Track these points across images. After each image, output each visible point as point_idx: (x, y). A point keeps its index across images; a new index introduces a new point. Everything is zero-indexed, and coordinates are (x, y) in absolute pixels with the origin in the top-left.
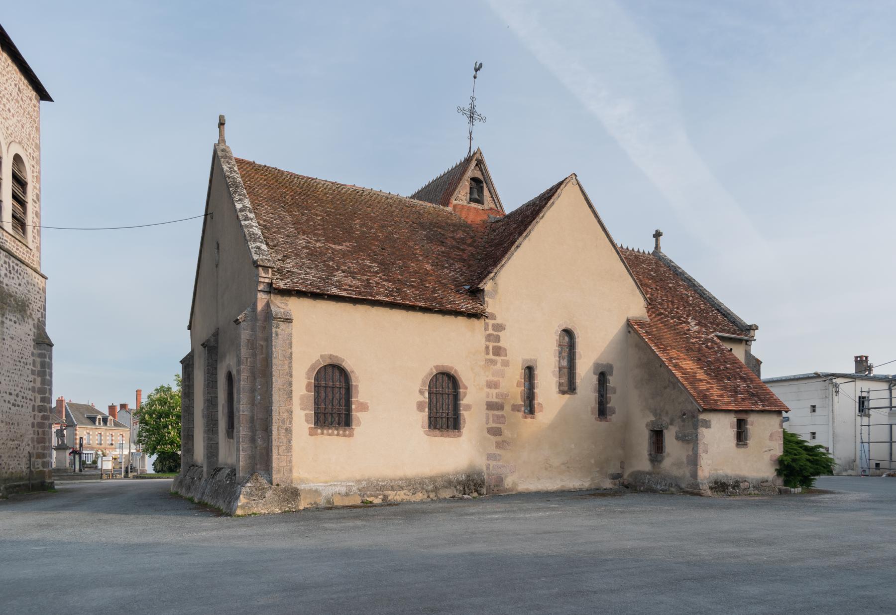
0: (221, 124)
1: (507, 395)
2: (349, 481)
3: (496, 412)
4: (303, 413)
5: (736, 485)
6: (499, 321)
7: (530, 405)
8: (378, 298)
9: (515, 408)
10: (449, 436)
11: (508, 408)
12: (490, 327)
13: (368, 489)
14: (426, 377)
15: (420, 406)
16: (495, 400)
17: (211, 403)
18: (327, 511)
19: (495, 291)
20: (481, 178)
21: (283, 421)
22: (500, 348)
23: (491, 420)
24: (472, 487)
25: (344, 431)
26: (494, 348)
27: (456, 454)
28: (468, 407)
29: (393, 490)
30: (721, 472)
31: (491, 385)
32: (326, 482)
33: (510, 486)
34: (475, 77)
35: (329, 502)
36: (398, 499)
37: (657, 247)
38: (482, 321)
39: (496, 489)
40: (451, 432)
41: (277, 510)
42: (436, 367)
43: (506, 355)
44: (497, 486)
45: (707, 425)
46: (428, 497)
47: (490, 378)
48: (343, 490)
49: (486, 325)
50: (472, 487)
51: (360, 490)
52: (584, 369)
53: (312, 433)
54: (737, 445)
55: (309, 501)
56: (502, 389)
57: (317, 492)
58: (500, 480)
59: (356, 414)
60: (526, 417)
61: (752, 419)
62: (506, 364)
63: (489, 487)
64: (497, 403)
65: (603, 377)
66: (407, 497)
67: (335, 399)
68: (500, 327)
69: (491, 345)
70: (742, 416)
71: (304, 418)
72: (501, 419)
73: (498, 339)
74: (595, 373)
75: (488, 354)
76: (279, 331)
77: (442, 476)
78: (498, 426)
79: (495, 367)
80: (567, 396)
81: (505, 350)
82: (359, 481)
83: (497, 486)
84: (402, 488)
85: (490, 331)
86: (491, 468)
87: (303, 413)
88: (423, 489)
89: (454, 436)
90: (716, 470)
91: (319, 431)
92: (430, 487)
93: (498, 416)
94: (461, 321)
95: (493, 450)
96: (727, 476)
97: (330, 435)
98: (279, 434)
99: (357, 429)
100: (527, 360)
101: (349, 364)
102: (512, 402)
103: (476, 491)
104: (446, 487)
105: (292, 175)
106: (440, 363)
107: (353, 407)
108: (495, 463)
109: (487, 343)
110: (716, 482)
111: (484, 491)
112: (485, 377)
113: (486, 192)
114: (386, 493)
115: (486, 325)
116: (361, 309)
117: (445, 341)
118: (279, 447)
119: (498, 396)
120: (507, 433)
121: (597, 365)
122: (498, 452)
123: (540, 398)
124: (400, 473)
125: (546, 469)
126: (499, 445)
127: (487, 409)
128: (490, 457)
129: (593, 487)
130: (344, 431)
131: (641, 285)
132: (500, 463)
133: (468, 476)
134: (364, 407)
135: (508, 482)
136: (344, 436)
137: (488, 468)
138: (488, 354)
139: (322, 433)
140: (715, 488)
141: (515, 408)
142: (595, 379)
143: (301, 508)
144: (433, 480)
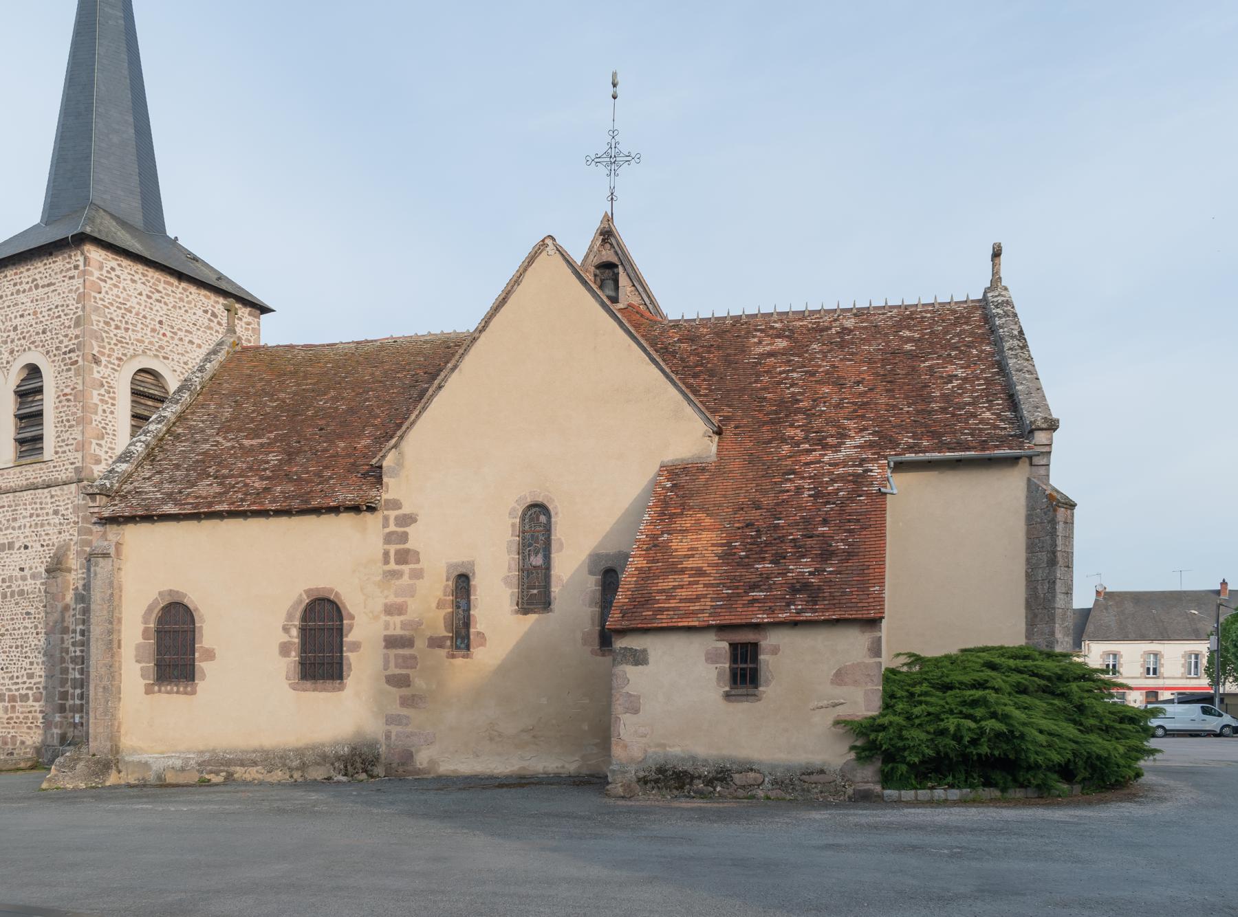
0: (996, 254)
2: (189, 752)
3: (401, 651)
5: (721, 776)
6: (406, 510)
7: (461, 635)
8: (218, 508)
10: (325, 690)
11: (421, 644)
12: (392, 521)
13: (208, 762)
14: (294, 607)
15: (284, 649)
16: (399, 632)
18: (158, 788)
19: (400, 464)
20: (615, 260)
21: (101, 678)
22: (407, 551)
23: (392, 664)
24: (359, 765)
25: (186, 688)
26: (397, 552)
27: (342, 715)
28: (356, 646)
29: (242, 765)
31: (390, 610)
32: (162, 753)
33: (425, 765)
34: (615, 97)
35: (159, 778)
36: (248, 777)
37: (996, 279)
38: (379, 516)
39: (401, 770)
40: (329, 684)
41: (83, 786)
42: (307, 592)
43: (418, 561)
44: (403, 764)
45: (639, 658)
46: (291, 777)
47: (392, 599)
48: (179, 763)
49: (386, 519)
50: (359, 765)
51: (199, 765)
52: (569, 565)
54: (727, 696)
55: (136, 775)
56: (412, 614)
57: (146, 765)
58: (408, 756)
59: (202, 665)
60: (453, 656)
62: (417, 575)
63: (388, 767)
64: (402, 637)
65: (609, 577)
66: (260, 776)
67: (176, 648)
68: (408, 520)
69: (392, 549)
70: (749, 637)
71: (139, 673)
73: (404, 538)
74: (591, 573)
75: (386, 562)
76: (98, 569)
78: (404, 672)
79: (398, 582)
80: (532, 617)
81: (417, 553)
82: (202, 752)
83: (403, 764)
84: (255, 763)
86: (393, 737)
88: (284, 765)
89: (334, 690)
90: (664, 746)
91: (156, 688)
92: (296, 763)
93: (404, 657)
94: (346, 519)
95: (396, 709)
96: (694, 759)
97: (168, 693)
98: (96, 694)
99: (201, 685)
100: (456, 566)
101: (194, 599)
102: (429, 634)
103: (366, 771)
104: (319, 764)
106: (313, 584)
107: (197, 655)
108: (399, 729)
109: (387, 547)
110: (661, 770)
112: (379, 601)
113: (623, 280)
114: (232, 769)
115: (386, 519)
116: (207, 524)
118: (96, 709)
119: (404, 625)
120: (419, 683)
121: (595, 558)
122: (405, 712)
123: (482, 619)
124: (255, 743)
125: (491, 739)
126: (406, 702)
127: (386, 647)
128: (391, 720)
129: (585, 771)
130: (186, 688)
131: (690, 391)
132: (409, 729)
133: (354, 749)
134: (210, 655)
135: (422, 758)
136: (186, 693)
137: (388, 737)
138: (386, 562)
139: (160, 691)
140: (657, 781)
141: (435, 643)
142: (592, 583)
143: (108, 784)
144: (300, 752)
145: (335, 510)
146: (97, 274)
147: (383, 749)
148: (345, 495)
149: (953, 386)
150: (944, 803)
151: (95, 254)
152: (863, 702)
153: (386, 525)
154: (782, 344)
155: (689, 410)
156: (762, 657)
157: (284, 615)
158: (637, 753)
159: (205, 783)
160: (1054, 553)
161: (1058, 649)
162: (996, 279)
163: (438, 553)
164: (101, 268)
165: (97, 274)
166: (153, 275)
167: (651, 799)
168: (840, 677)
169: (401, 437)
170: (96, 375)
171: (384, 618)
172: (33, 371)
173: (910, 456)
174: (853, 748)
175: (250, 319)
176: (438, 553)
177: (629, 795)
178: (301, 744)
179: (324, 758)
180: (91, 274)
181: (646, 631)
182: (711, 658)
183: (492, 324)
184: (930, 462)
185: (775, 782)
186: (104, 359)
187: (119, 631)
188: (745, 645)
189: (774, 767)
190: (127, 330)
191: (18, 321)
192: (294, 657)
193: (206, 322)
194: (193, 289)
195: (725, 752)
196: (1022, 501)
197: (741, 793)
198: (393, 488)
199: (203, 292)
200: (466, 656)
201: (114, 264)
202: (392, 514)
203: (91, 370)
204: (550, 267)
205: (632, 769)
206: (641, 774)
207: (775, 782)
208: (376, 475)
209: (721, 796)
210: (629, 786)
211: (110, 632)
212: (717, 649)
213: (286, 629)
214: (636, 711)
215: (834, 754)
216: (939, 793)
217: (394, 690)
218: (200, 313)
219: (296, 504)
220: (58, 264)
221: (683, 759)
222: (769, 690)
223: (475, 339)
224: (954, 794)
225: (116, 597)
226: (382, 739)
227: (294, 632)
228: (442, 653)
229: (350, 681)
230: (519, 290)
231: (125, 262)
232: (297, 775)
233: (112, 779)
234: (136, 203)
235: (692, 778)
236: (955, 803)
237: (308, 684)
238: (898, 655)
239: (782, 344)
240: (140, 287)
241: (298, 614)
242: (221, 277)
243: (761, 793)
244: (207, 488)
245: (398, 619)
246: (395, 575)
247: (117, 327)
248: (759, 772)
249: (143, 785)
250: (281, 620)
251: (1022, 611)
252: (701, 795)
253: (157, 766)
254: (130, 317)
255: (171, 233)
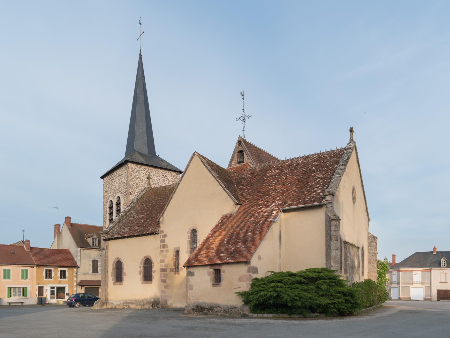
0: (351, 131)
1: (168, 265)
4: (112, 278)
5: (211, 308)
6: (164, 233)
8: (125, 235)
9: (171, 270)
11: (168, 270)
14: (142, 261)
15: (140, 272)
16: (163, 267)
17: (363, 263)
19: (163, 220)
20: (242, 149)
22: (165, 245)
26: (163, 245)
27: (151, 291)
30: (201, 301)
34: (243, 99)
36: (132, 307)
37: (351, 139)
42: (145, 257)
47: (162, 258)
48: (119, 303)
49: (160, 236)
53: (114, 284)
54: (213, 285)
57: (112, 303)
58: (166, 302)
59: (124, 277)
60: (175, 274)
61: (224, 268)
62: (167, 251)
68: (165, 236)
69: (162, 244)
70: (217, 268)
72: (166, 276)
73: (164, 241)
75: (161, 248)
77: (146, 300)
78: (165, 278)
84: (134, 304)
85: (162, 238)
87: (112, 278)
90: (198, 299)
92: (142, 304)
95: (163, 289)
96: (205, 303)
99: (124, 282)
102: (170, 268)
105: (306, 158)
110: (198, 306)
111: (160, 306)
116: (125, 240)
117: (146, 246)
119: (165, 265)
122: (165, 290)
126: (166, 287)
128: (162, 292)
132: (166, 295)
135: (169, 303)
137: (162, 297)
138: (161, 248)
140: (196, 309)
141: (171, 270)
144: (143, 301)
145: (148, 234)
146: (131, 170)
147: (160, 300)
148: (151, 230)
149: (313, 181)
150: (267, 318)
151: (130, 165)
152: (246, 287)
153: (160, 238)
154: (277, 171)
155: (229, 198)
156: (221, 273)
157: (140, 263)
158: (193, 302)
159: (124, 308)
160: (330, 236)
161: (332, 269)
162: (351, 139)
163: (172, 246)
164: (132, 169)
165: (131, 170)
166: (147, 168)
167: (195, 315)
168: (240, 279)
169: (163, 213)
170: (131, 198)
171: (160, 263)
172: (119, 197)
173: (287, 208)
174: (243, 301)
175: (177, 176)
176: (172, 246)
177: (189, 313)
178: (143, 298)
179: (148, 303)
180: (129, 171)
181: (193, 266)
182: (209, 274)
183: (183, 179)
184: (293, 209)
185: (224, 311)
186: (133, 193)
187: (108, 269)
188: (217, 270)
189: (224, 306)
190: (139, 184)
191: (116, 185)
192: (142, 275)
193: (163, 178)
194: (159, 170)
195: (212, 302)
196: (324, 219)
197: (215, 313)
198: (162, 227)
199: (162, 170)
200: (178, 274)
201: (136, 167)
202: (162, 234)
203: (130, 197)
204: (196, 159)
205: (191, 306)
206: (193, 307)
207: (225, 311)
208: (158, 224)
209: (210, 314)
210: (189, 311)
211: (105, 269)
212: (210, 271)
213: (140, 267)
214: (192, 289)
215: (238, 302)
216: (265, 315)
217: (162, 283)
218: (161, 176)
219: (140, 233)
220: (123, 169)
221: (202, 303)
222: (223, 283)
223: (179, 184)
224: (271, 315)
225: (106, 260)
226: (160, 298)
227: (142, 268)
228: (173, 273)
229: (153, 281)
230: (189, 168)
231: (139, 166)
232: (142, 307)
233: (105, 307)
234: (146, 148)
235: (205, 309)
236: (270, 318)
237: (145, 282)
238: (268, 272)
239: (277, 171)
240: (143, 172)
241: (143, 263)
242: (169, 164)
243: (219, 314)
244: (127, 230)
245: (163, 264)
246: (162, 251)
247: (137, 184)
248: (220, 307)
249: (112, 309)
250: (139, 265)
251: (325, 256)
252: (206, 314)
253: (115, 304)
254: (141, 181)
255: (157, 154)
